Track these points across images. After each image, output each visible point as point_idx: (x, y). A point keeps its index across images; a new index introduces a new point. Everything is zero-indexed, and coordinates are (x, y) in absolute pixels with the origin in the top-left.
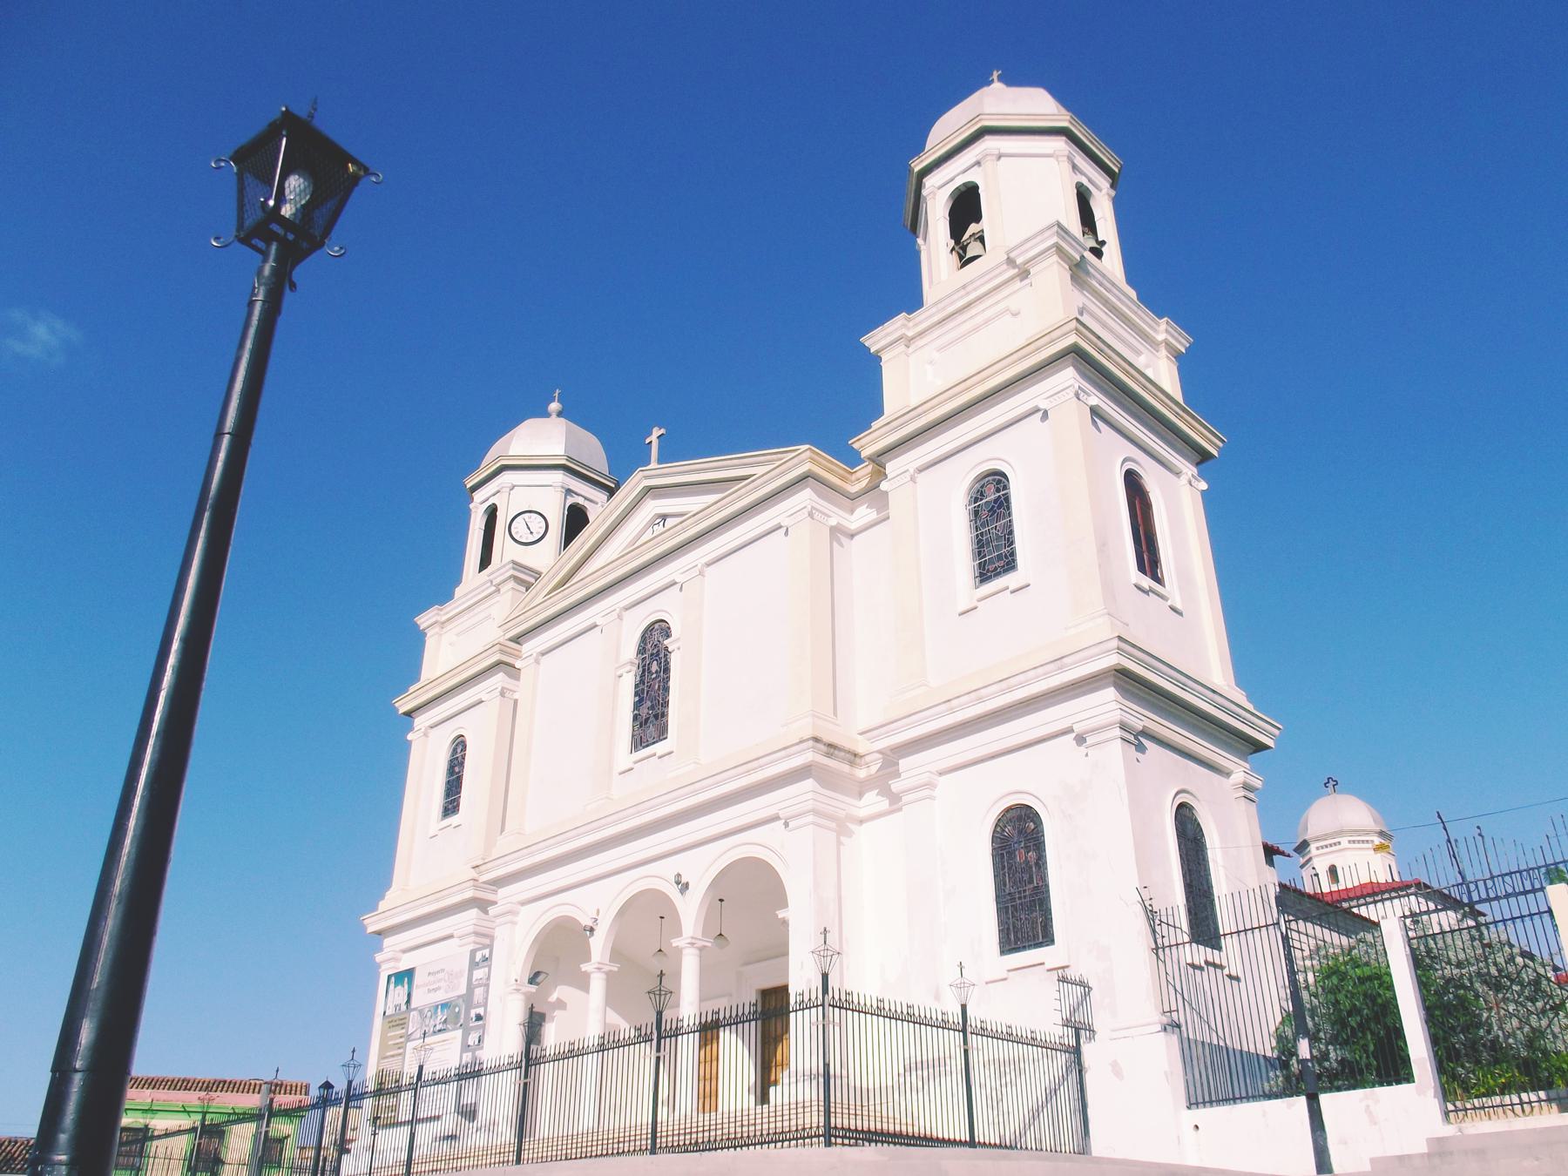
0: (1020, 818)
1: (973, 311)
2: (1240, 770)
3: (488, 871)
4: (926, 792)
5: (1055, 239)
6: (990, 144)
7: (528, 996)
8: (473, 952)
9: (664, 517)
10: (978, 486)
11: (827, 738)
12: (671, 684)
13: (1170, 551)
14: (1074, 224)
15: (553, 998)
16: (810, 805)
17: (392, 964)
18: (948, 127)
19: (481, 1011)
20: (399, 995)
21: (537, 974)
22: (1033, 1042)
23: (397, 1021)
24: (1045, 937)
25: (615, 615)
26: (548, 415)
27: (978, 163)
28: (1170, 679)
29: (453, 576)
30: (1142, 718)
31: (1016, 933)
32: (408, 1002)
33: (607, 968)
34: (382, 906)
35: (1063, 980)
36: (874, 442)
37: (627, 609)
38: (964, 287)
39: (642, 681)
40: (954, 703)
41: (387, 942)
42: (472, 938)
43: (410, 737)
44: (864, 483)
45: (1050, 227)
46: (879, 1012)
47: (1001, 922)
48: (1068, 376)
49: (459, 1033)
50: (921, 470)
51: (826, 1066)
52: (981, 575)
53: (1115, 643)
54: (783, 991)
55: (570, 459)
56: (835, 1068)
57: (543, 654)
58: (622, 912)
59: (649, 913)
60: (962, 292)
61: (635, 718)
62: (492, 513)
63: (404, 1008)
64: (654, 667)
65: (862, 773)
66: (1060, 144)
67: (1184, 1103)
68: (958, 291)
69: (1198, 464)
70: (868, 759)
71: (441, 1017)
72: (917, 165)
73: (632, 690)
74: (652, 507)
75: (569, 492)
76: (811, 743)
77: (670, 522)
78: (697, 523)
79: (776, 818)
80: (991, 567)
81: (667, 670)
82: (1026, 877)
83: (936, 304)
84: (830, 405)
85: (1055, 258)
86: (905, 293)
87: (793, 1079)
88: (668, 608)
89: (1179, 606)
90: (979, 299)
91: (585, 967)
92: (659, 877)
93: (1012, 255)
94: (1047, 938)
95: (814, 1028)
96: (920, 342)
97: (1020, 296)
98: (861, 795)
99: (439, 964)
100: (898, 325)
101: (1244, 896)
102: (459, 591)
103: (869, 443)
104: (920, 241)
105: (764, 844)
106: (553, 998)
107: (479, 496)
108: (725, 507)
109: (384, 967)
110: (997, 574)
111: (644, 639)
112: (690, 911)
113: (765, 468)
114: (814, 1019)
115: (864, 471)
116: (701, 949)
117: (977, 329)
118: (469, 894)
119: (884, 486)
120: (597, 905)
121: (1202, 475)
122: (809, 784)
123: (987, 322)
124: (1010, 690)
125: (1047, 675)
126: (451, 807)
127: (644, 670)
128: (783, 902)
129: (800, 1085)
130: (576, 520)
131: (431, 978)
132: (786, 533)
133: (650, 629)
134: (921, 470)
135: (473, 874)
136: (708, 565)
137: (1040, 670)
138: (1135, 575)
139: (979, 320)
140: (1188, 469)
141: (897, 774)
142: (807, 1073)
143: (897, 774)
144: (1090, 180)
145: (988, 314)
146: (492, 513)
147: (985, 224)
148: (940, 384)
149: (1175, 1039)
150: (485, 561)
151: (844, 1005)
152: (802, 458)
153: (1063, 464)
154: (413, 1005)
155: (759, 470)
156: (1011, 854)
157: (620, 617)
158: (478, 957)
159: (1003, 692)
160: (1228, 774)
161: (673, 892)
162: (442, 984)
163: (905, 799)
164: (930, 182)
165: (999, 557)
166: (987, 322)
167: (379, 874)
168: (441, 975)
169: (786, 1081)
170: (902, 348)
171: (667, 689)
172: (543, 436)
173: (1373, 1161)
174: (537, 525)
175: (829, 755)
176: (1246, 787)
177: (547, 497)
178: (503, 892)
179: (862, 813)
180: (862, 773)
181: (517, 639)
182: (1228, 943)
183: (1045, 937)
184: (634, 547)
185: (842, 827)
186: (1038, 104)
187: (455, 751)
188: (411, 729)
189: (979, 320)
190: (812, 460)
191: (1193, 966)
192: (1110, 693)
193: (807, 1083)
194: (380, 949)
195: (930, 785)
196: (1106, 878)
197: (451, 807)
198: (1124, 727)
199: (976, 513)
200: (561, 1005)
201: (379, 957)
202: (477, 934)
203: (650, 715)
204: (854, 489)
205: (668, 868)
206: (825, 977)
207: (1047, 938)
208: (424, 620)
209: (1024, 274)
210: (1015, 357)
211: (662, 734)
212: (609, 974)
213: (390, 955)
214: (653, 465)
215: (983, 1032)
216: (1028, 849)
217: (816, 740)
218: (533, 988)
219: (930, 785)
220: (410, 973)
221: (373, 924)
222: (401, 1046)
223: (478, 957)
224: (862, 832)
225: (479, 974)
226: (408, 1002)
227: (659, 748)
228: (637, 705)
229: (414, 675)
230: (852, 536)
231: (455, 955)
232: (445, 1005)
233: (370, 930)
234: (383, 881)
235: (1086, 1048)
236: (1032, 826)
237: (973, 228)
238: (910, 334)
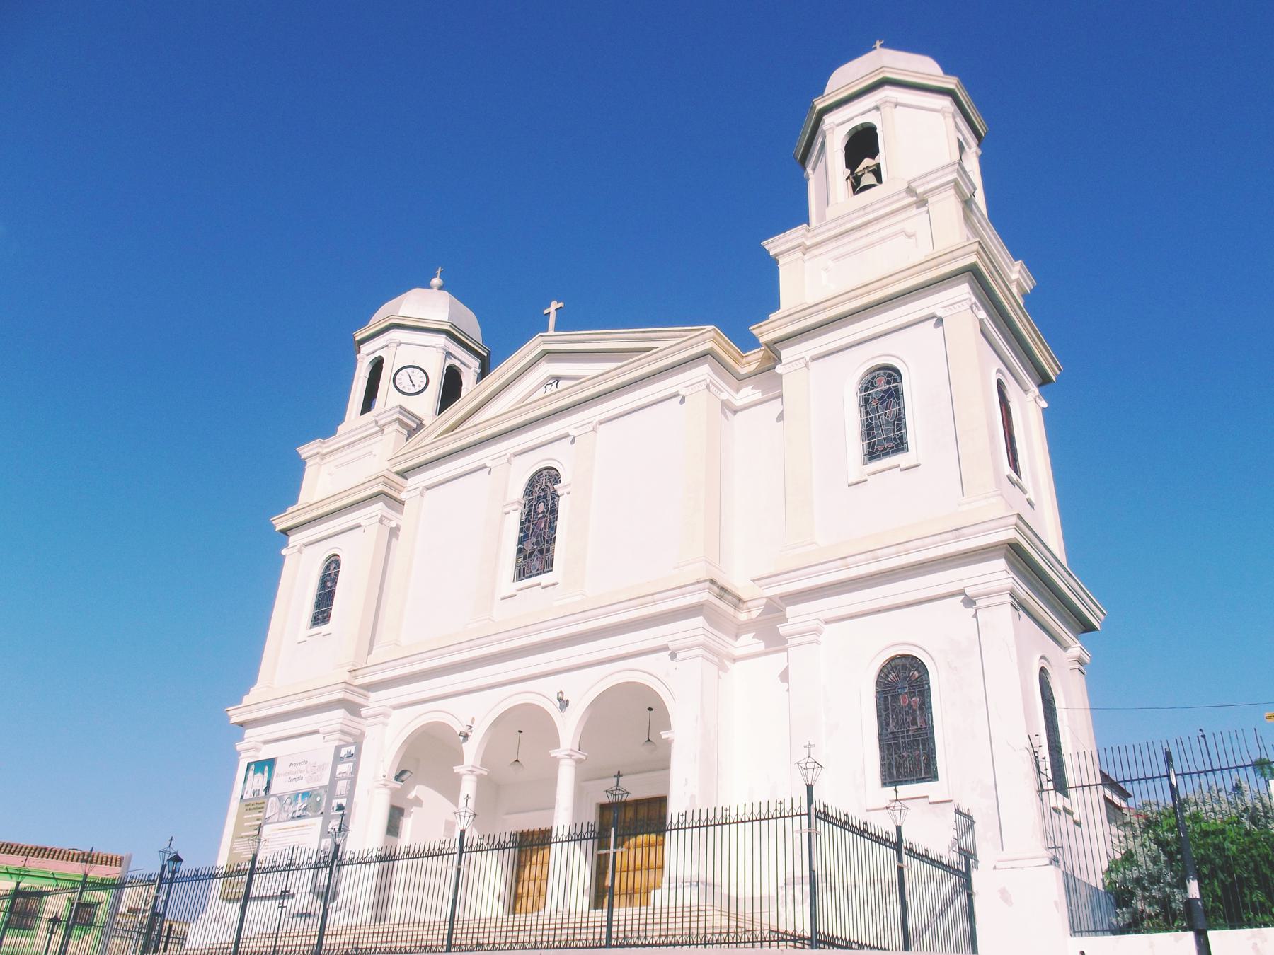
0: (904, 667)
1: (869, 230)
2: (1076, 649)
3: (364, 675)
4: (813, 637)
5: (955, 175)
6: (888, 92)
7: (394, 793)
8: (338, 749)
9: (558, 379)
10: (869, 377)
11: (721, 582)
12: (559, 523)
15: (412, 795)
16: (700, 639)
17: (252, 753)
18: (844, 78)
19: (343, 802)
20: (258, 781)
21: (403, 772)
23: (254, 805)
24: (928, 772)
25: (505, 459)
26: (429, 287)
27: (877, 108)
28: (1045, 559)
29: (340, 417)
30: (1024, 591)
31: (898, 768)
32: (267, 788)
33: (478, 772)
34: (247, 700)
36: (774, 330)
37: (516, 455)
38: (863, 208)
39: (528, 520)
40: (850, 560)
41: (248, 733)
42: (338, 735)
43: (284, 552)
44: (753, 367)
46: (844, 825)
47: (882, 758)
48: (963, 292)
49: (319, 820)
50: (814, 359)
51: (811, 871)
52: (870, 453)
53: (1014, 519)
54: (661, 801)
55: (453, 326)
56: (819, 869)
57: (428, 488)
58: (496, 723)
59: (524, 728)
60: (862, 212)
61: (519, 551)
62: (378, 365)
63: (262, 793)
64: (541, 508)
65: (743, 617)
66: (945, 103)
67: (1068, 931)
68: (857, 210)
69: (1039, 386)
70: (750, 604)
71: (301, 804)
72: (820, 104)
73: (517, 527)
74: (547, 369)
75: (449, 354)
76: (708, 584)
77: (563, 384)
78: (595, 385)
79: (665, 648)
80: (881, 448)
81: (554, 511)
82: (909, 719)
83: (835, 220)
84: (733, 295)
85: (952, 192)
86: (796, 214)
87: (673, 885)
89: (1033, 500)
90: (876, 219)
91: (457, 769)
92: (543, 694)
93: (913, 185)
95: (797, 836)
96: (815, 252)
97: (916, 220)
98: (737, 637)
99: (304, 757)
100: (795, 235)
102: (341, 429)
103: (767, 331)
104: (809, 170)
106: (412, 795)
107: (365, 349)
108: (625, 373)
109: (243, 755)
110: (886, 453)
111: (531, 483)
112: (569, 727)
113: (666, 343)
114: (797, 827)
115: (754, 358)
116: (579, 761)
117: (871, 245)
118: (339, 695)
119: (779, 369)
120: (474, 712)
121: (1044, 395)
122: (699, 621)
123: (882, 240)
124: (907, 552)
126: (322, 613)
127: (530, 510)
128: (667, 726)
129: (680, 891)
130: (452, 387)
131: (294, 769)
132: (683, 401)
133: (538, 474)
134: (814, 359)
135: (346, 677)
136: (601, 423)
137: (937, 538)
140: (1034, 390)
141: (785, 620)
142: (687, 878)
143: (785, 620)
146: (378, 365)
147: (881, 158)
148: (832, 289)
150: (367, 405)
151: (823, 816)
152: (706, 337)
153: (954, 367)
154: (273, 790)
156: (895, 698)
157: (509, 461)
158: (344, 752)
159: (899, 554)
160: (1065, 649)
161: (552, 708)
162: (304, 775)
163: (791, 641)
164: (829, 120)
165: (888, 440)
166: (882, 240)
167: (245, 670)
168: (304, 767)
169: (665, 885)
170: (800, 254)
171: (554, 529)
172: (429, 304)
174: (419, 379)
175: (720, 597)
176: (1080, 661)
177: (431, 356)
178: (374, 696)
179: (737, 652)
180: (743, 617)
181: (403, 474)
182: (1072, 792)
183: (928, 772)
184: (523, 404)
185: (722, 660)
186: (925, 67)
187: (328, 568)
188: (285, 545)
190: (715, 340)
191: (1056, 810)
192: (1001, 564)
193: (687, 890)
194: (242, 739)
195: (817, 631)
196: (984, 726)
197: (322, 613)
198: (1012, 594)
199: (866, 400)
200: (418, 802)
201: (239, 746)
202: (342, 732)
203: (536, 546)
204: (743, 371)
206: (810, 788)
208: (305, 451)
209: (922, 202)
210: (912, 271)
211: (548, 566)
212: (480, 777)
213: (252, 744)
214: (551, 332)
215: (911, 852)
216: (912, 694)
217: (713, 582)
218: (398, 785)
219: (817, 631)
220: (271, 763)
221: (236, 715)
223: (344, 752)
224: (735, 668)
225: (344, 768)
226: (267, 788)
227: (544, 579)
228: (521, 540)
229: (293, 498)
230: (735, 412)
231: (320, 751)
232: (306, 794)
233: (233, 720)
234: (248, 675)
235: (975, 874)
236: (916, 674)
238: (808, 243)
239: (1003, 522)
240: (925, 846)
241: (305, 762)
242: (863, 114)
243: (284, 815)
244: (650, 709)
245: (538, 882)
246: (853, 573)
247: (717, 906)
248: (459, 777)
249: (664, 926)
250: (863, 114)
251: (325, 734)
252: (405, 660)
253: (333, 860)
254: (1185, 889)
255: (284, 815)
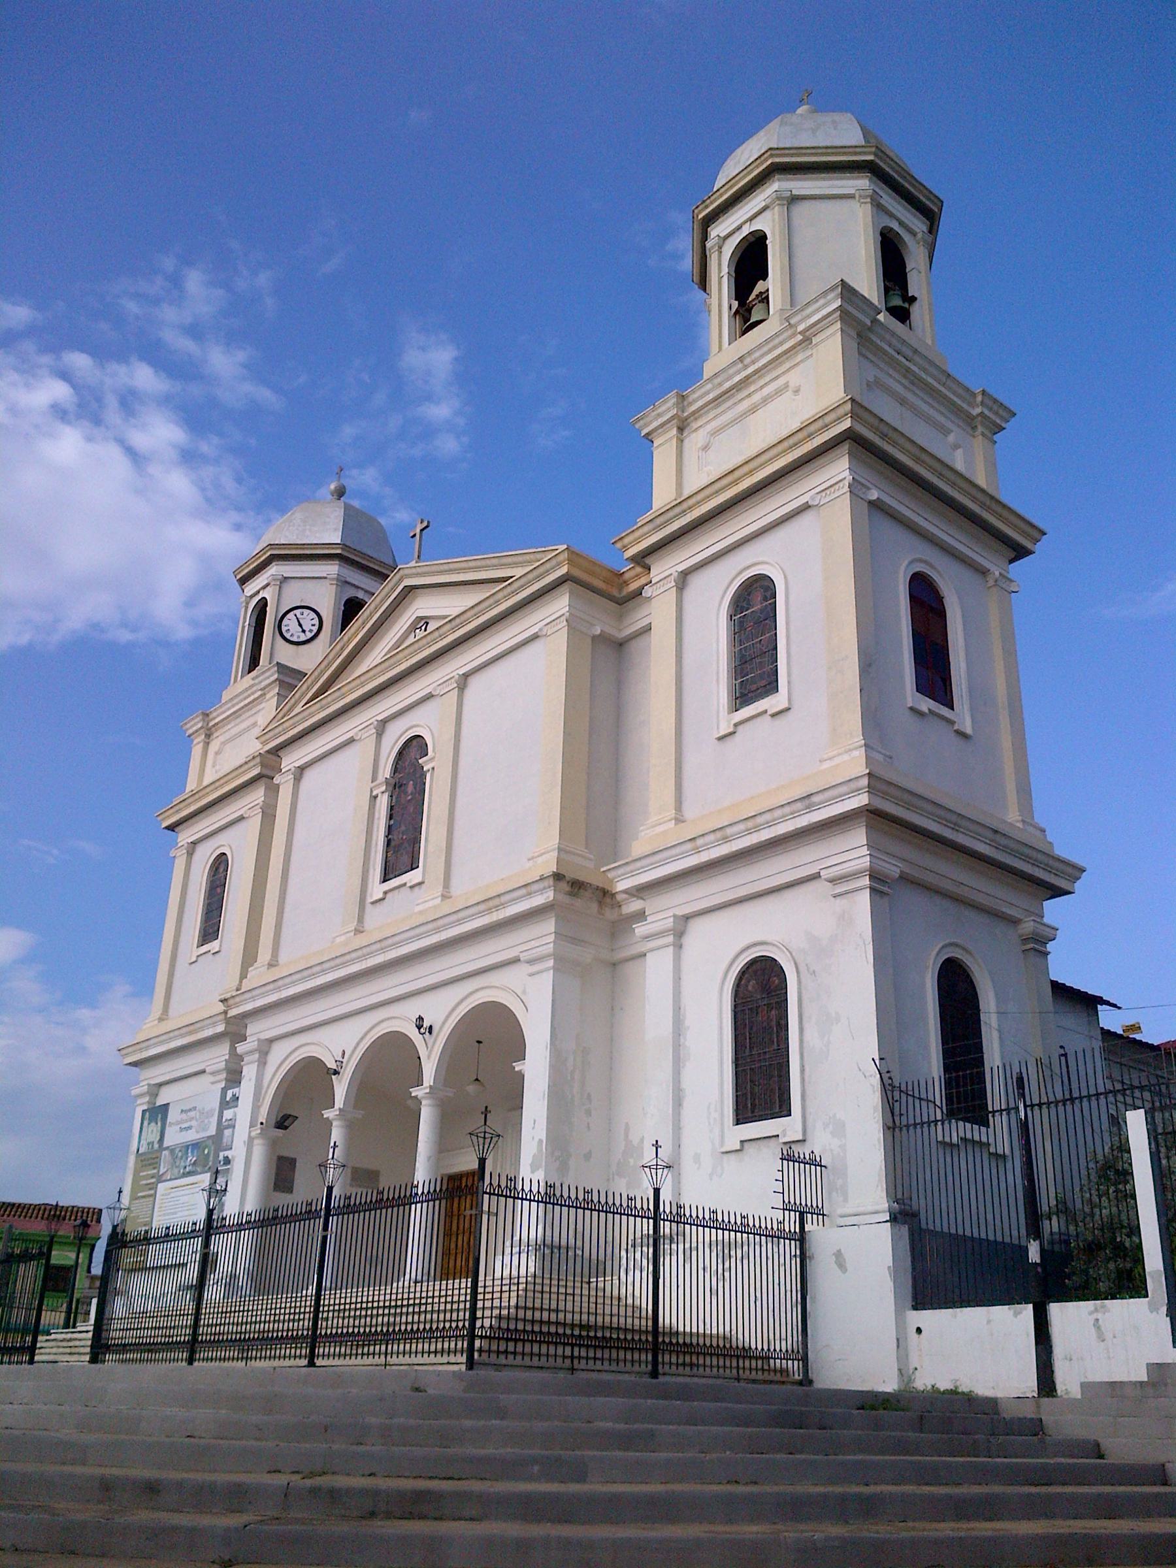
11: (571, 875)
13: (963, 665)
14: (869, 284)
22: (744, 1228)
35: (788, 1158)
38: (741, 359)
45: (832, 289)
59: (391, 1059)
63: (156, 1146)
68: (734, 363)
71: (191, 1158)
87: (516, 1250)
88: (428, 723)
94: (784, 1110)
101: (1080, 1056)
105: (499, 989)
117: (753, 409)
124: (757, 829)
125: (794, 815)
126: (210, 931)
129: (524, 1256)
130: (351, 609)
131: (184, 1116)
138: (910, 695)
139: (756, 398)
141: (148, 1102)
142: (532, 1242)
144: (901, 223)
145: (766, 391)
149: (905, 1230)
154: (166, 1144)
155: (518, 572)
159: (749, 832)
162: (194, 1123)
165: (761, 676)
168: (192, 1114)
173: (1083, 1385)
189: (756, 398)
197: (210, 931)
205: (412, 1009)
207: (784, 1110)
210: (786, 444)
211: (771, 686)
222: (154, 1187)
225: (228, 1114)
226: (161, 1140)
237: (760, 287)
239: (853, 785)
240: (710, 1204)
241: (195, 1108)
242: (751, 219)
243: (176, 1171)
244: (479, 1042)
245: (467, 1235)
246: (704, 857)
247: (578, 1270)
248: (328, 1123)
249: (562, 1290)
250: (751, 219)
251: (213, 1073)
252: (271, 986)
253: (212, 1226)
254: (1043, 1251)
255: (176, 1171)
